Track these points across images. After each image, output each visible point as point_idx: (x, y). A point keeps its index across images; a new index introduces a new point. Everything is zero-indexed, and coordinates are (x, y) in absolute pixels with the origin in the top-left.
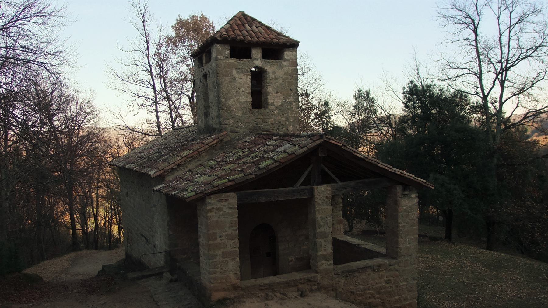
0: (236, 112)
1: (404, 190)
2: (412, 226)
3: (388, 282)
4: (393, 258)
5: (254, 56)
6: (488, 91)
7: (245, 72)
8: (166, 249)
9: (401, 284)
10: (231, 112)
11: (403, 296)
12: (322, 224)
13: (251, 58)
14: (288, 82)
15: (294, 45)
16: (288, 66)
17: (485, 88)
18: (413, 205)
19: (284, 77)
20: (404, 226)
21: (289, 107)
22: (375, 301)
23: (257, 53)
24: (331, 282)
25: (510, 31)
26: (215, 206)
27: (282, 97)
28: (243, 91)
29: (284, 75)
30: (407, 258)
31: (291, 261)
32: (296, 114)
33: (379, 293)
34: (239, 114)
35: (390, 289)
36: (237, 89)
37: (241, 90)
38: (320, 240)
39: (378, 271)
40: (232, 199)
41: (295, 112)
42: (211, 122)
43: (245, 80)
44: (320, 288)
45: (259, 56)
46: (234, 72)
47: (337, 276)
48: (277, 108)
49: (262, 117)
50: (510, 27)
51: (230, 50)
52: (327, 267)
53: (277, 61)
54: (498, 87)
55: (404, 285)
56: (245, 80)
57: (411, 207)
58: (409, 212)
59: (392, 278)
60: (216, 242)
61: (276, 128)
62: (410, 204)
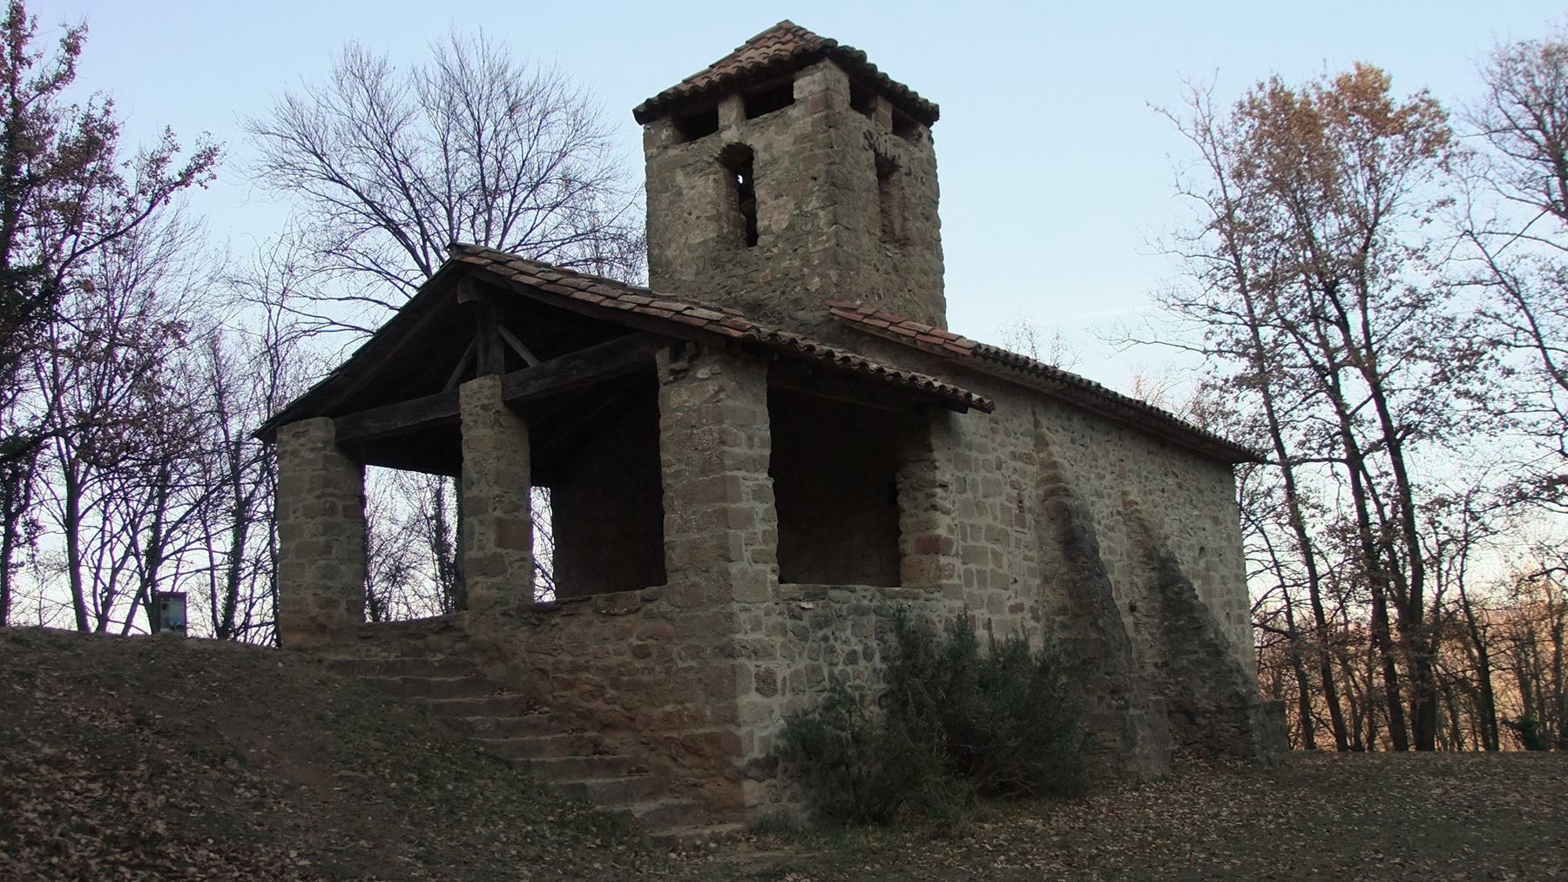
0: (681, 273)
1: (675, 357)
2: (704, 472)
3: (641, 653)
7: (702, 170)
9: (681, 664)
11: (687, 705)
12: (475, 476)
14: (804, 160)
18: (705, 402)
19: (793, 149)
20: (677, 475)
21: (809, 226)
22: (606, 707)
23: (729, 113)
24: (493, 635)
27: (791, 205)
28: (698, 218)
29: (795, 143)
30: (694, 579)
32: (827, 241)
33: (616, 685)
34: (688, 276)
35: (646, 678)
37: (693, 217)
38: (471, 519)
39: (608, 614)
41: (825, 238)
43: (701, 189)
45: (734, 116)
46: (680, 177)
48: (778, 237)
49: (742, 272)
52: (486, 593)
53: (777, 113)
55: (692, 668)
56: (701, 189)
57: (698, 410)
59: (654, 642)
60: (289, 522)
61: (778, 293)
62: (695, 401)
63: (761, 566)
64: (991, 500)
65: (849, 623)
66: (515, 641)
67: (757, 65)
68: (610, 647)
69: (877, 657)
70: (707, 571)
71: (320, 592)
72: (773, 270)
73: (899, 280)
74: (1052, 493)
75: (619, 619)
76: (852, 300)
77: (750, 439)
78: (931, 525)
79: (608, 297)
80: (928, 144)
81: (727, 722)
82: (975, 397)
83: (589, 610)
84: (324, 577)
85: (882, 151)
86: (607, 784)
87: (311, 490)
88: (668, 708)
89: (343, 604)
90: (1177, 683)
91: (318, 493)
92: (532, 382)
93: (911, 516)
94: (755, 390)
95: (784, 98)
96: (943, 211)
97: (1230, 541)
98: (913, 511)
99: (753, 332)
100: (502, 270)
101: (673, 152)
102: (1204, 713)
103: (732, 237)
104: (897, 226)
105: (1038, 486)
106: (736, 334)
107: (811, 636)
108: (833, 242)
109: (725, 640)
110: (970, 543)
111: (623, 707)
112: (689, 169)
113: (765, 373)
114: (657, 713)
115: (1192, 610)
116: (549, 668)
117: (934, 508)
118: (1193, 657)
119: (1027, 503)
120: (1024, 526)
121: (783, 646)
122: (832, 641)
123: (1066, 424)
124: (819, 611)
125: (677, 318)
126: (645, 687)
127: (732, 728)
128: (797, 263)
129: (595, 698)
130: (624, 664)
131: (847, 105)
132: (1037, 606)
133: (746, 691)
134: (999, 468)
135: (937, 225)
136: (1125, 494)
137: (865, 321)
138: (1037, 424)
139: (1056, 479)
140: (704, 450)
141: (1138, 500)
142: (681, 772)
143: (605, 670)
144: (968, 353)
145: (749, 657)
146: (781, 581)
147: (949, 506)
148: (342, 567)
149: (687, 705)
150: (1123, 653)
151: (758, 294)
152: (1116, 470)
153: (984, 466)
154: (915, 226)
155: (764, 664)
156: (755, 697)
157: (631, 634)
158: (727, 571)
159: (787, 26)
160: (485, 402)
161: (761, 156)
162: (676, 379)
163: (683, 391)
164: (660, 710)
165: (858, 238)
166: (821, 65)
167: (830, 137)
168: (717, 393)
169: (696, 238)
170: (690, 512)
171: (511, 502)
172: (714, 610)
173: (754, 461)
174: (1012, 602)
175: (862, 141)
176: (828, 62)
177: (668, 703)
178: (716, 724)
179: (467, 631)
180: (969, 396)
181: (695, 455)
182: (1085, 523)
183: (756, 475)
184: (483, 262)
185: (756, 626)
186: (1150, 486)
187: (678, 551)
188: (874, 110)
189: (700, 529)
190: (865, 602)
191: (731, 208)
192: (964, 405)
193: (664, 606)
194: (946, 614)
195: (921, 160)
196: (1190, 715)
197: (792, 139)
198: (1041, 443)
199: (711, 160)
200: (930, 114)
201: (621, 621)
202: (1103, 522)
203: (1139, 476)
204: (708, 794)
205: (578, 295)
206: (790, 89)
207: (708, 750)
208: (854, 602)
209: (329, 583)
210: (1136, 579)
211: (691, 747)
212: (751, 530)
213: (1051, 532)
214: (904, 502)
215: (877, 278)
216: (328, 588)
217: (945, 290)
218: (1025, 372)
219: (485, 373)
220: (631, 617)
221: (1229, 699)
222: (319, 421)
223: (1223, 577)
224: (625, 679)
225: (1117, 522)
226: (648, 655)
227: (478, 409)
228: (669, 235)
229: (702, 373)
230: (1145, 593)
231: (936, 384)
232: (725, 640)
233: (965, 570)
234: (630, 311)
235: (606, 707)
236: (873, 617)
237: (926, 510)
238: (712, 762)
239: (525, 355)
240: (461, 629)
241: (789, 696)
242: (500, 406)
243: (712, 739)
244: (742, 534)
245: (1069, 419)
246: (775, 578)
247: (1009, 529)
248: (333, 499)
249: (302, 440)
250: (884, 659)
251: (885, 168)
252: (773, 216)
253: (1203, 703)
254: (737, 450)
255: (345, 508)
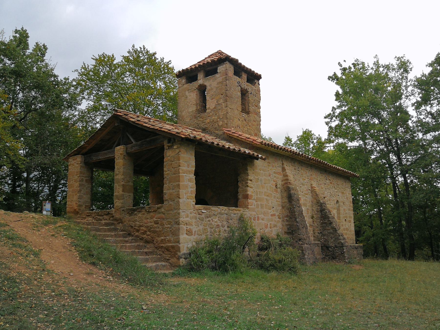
1: (169, 143)
2: (174, 174)
3: (156, 223)
9: (166, 226)
10: (183, 120)
16: (415, 81)
20: (168, 174)
22: (147, 237)
23: (201, 76)
26: (72, 163)
27: (216, 102)
28: (191, 104)
29: (217, 84)
30: (171, 203)
32: (225, 111)
34: (188, 120)
35: (157, 230)
36: (188, 103)
37: (190, 104)
40: (79, 159)
46: (187, 93)
47: (124, 212)
49: (202, 120)
57: (174, 157)
58: (172, 161)
59: (159, 220)
63: (190, 200)
64: (266, 185)
65: (217, 217)
66: (125, 218)
67: (208, 62)
68: (148, 220)
69: (226, 227)
70: (174, 201)
71: (77, 202)
72: (210, 120)
73: (246, 123)
74: (286, 183)
75: (152, 213)
76: (231, 128)
77: (188, 165)
78: (246, 191)
79: (152, 125)
80: (258, 85)
81: (177, 242)
82: (260, 156)
83: (144, 210)
84: (79, 198)
85: (243, 87)
86: (142, 258)
87: (76, 175)
88: (162, 238)
89: (84, 206)
90: (324, 238)
91: (78, 176)
92: (134, 148)
93: (241, 188)
94: (191, 152)
95: (215, 72)
96: (261, 104)
97: (348, 199)
98: (242, 187)
99: (188, 136)
100: (126, 117)
101: (185, 86)
102: (331, 247)
103: (200, 110)
104: (247, 108)
105: (282, 181)
106: (183, 136)
107: (205, 220)
108: (226, 112)
109: (177, 220)
110: (259, 196)
111: (151, 237)
112: (190, 91)
113: (194, 148)
114: (159, 239)
115: (328, 218)
116: (133, 225)
117: (248, 186)
118: (329, 231)
119: (278, 186)
120: (277, 192)
121: (195, 222)
122: (211, 222)
123: (293, 164)
124: (208, 213)
125: (169, 132)
126: (157, 232)
127: (178, 244)
128: (216, 117)
129: (144, 234)
130: (152, 226)
131: (232, 74)
132: (280, 215)
133: (182, 234)
134: (270, 176)
135: (259, 108)
136: (311, 184)
137: (233, 134)
138: (283, 164)
139: (287, 180)
140: (175, 168)
141: (316, 186)
142: (164, 255)
143: (147, 227)
144: (259, 144)
145: (184, 225)
146: (196, 204)
147: (252, 186)
148: (84, 196)
149: (167, 237)
150: (304, 229)
151: (206, 126)
152: (309, 178)
153: (265, 175)
154: (252, 108)
155: (189, 227)
156: (185, 236)
157: (154, 217)
158: (179, 201)
159: (219, 52)
160: (121, 152)
161: (208, 88)
162: (169, 148)
163: (170, 152)
164: (160, 238)
165: (233, 111)
166: (225, 63)
167: (227, 83)
168: (179, 152)
169: (190, 110)
170: (170, 185)
171: (127, 180)
172: (175, 211)
173: (189, 171)
174: (272, 213)
175: (237, 84)
176: (227, 62)
177: (162, 236)
178: (174, 243)
179: (114, 215)
180: (258, 155)
181: (173, 169)
182: (296, 192)
183: (190, 175)
184: (121, 114)
185: (187, 216)
186: (320, 182)
187: (167, 195)
188: (241, 76)
189: (173, 189)
190: (223, 211)
191: (201, 102)
192: (257, 158)
193: (163, 210)
194: (249, 216)
195: (255, 90)
196: (327, 248)
197: (217, 83)
198: (284, 169)
199: (195, 88)
200: (258, 77)
201: (152, 214)
202: (304, 192)
203: (317, 180)
204: (171, 262)
205: (145, 125)
206: (217, 69)
207: (172, 250)
208: (219, 211)
209: (80, 200)
210: (314, 209)
211: (167, 249)
212: (187, 190)
213: (285, 194)
214: (240, 184)
215: (239, 123)
216: (80, 202)
217: (261, 126)
218: (279, 150)
219: (164, 143)
220: (154, 213)
221: (339, 243)
222: (80, 156)
223: (344, 209)
224: (152, 229)
225: (308, 192)
226: (158, 223)
227: (119, 154)
228: (183, 109)
229: (175, 147)
230: (316, 213)
231: (247, 152)
232: (177, 220)
233: (257, 204)
234: (157, 129)
235: (147, 237)
236: (225, 215)
237: (245, 187)
238: (173, 253)
239: (132, 140)
240: (112, 214)
241: (196, 236)
242: (125, 154)
243: (173, 247)
244: (184, 191)
245: (294, 163)
246: (194, 203)
247: (272, 193)
248: (83, 177)
249: (75, 161)
250: (228, 227)
251: (244, 93)
252: (210, 104)
253: (331, 245)
254: (184, 168)
255: (86, 180)
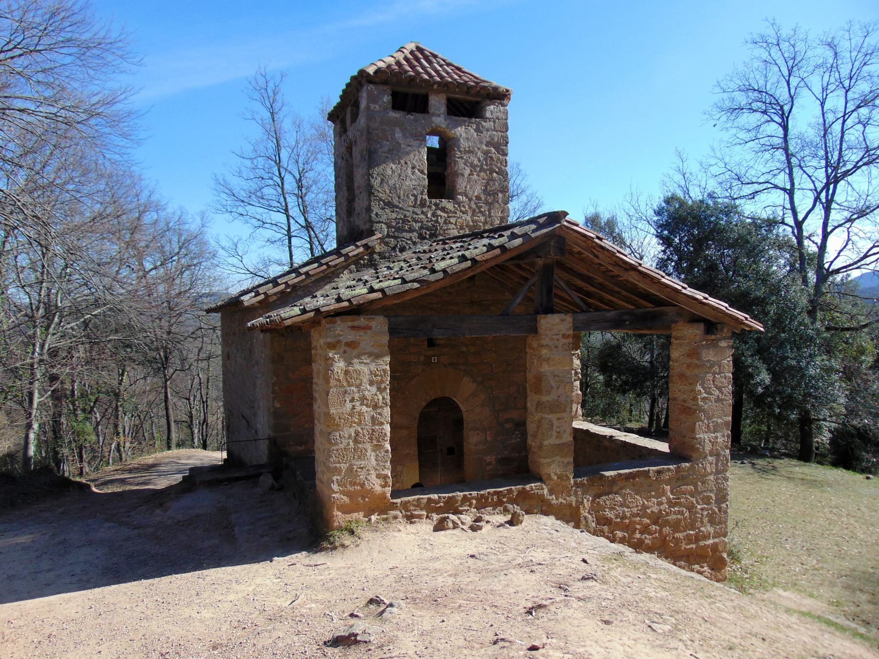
4: (686, 459)
5: (433, 110)
6: (804, 213)
8: (269, 435)
13: (428, 112)
15: (500, 96)
17: (798, 210)
25: (844, 121)
31: (490, 464)
42: (357, 223)
44: (546, 509)
46: (398, 135)
50: (844, 116)
51: (392, 95)
54: (819, 211)
